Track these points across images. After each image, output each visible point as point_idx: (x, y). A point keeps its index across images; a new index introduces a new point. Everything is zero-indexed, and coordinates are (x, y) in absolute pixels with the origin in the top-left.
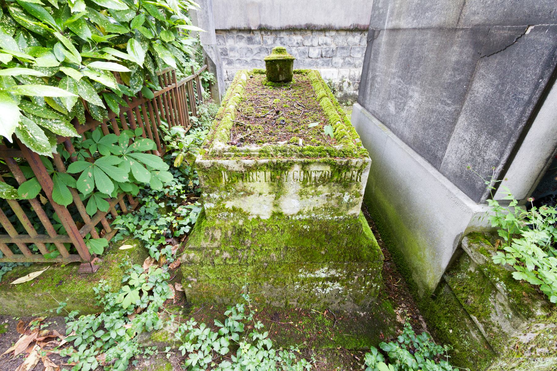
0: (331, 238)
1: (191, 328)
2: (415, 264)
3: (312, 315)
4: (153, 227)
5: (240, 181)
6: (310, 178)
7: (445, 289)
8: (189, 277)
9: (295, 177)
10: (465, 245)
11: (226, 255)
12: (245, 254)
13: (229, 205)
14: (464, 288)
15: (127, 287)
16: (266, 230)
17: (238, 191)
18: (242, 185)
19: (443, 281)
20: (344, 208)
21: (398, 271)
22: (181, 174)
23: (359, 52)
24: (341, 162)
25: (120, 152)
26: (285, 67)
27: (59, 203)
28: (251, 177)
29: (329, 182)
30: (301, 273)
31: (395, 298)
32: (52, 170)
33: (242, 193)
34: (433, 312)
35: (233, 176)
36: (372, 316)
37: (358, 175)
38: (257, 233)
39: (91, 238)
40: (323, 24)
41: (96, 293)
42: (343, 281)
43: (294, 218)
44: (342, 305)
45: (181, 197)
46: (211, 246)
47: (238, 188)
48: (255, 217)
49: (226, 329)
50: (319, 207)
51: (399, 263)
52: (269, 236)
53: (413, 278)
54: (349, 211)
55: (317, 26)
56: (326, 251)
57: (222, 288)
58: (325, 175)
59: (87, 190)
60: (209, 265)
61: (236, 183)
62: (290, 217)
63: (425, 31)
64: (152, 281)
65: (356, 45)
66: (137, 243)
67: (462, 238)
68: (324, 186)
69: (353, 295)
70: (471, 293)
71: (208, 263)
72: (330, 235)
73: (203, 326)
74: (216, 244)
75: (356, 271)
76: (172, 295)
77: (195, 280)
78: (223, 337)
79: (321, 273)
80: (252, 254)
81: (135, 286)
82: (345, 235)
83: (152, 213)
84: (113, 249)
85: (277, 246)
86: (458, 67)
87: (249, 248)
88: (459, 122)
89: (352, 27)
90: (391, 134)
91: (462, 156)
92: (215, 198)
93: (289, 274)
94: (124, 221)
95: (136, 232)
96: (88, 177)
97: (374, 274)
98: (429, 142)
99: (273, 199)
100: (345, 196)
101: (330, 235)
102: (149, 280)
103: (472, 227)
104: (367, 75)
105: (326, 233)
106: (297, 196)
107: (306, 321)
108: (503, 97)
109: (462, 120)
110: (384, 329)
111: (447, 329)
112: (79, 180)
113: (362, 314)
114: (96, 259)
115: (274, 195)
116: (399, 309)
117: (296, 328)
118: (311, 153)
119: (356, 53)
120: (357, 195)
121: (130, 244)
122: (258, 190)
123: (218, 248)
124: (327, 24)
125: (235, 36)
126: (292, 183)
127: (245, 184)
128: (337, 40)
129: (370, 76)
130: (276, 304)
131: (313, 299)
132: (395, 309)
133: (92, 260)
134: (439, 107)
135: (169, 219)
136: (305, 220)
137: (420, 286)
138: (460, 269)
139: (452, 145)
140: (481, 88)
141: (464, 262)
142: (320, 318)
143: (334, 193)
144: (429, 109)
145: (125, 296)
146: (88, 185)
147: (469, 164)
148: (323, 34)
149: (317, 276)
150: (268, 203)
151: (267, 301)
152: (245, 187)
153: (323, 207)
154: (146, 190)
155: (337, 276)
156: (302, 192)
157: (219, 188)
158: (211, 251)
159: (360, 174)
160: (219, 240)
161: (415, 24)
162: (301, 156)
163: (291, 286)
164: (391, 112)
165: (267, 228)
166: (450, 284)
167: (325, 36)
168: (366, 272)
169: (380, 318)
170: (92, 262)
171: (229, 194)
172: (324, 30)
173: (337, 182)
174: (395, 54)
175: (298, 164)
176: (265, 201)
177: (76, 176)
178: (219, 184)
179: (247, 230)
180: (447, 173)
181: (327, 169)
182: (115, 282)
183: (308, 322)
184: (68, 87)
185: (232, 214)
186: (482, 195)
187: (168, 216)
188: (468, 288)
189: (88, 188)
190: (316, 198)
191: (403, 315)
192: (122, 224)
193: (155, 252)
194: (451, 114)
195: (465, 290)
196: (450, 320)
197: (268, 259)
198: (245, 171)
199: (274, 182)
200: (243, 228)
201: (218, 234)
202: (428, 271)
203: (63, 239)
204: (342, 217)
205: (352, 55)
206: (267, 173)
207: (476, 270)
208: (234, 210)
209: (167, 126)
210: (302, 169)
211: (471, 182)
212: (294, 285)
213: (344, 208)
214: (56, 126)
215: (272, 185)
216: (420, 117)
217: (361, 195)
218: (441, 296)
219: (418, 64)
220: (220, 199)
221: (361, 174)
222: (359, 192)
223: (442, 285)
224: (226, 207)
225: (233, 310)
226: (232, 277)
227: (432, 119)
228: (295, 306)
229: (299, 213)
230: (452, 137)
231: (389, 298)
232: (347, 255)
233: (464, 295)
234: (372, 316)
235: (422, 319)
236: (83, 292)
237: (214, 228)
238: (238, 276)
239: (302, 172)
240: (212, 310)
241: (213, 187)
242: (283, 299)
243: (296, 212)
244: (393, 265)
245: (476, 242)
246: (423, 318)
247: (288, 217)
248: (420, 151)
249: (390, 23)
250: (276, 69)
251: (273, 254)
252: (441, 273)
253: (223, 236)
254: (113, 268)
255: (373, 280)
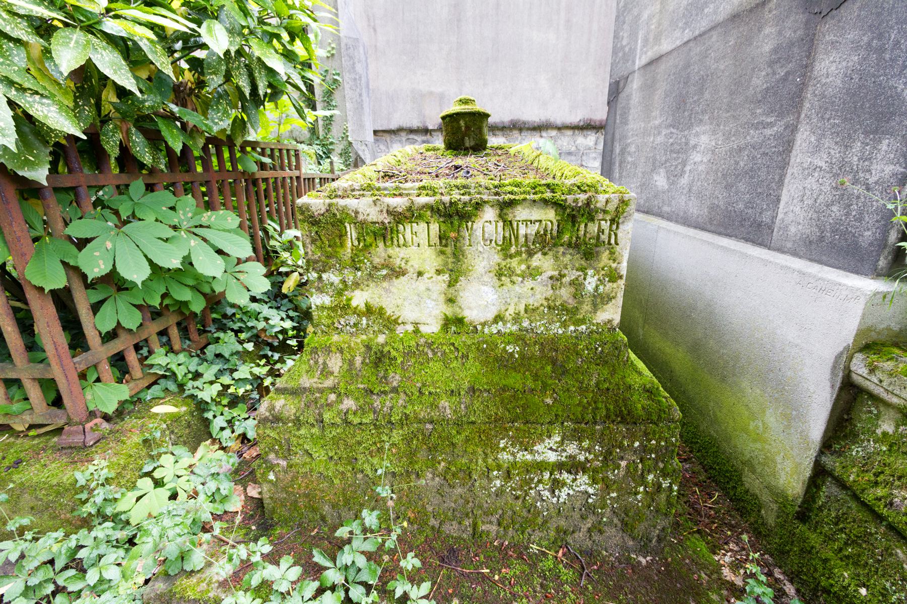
0: (563, 373)
1: (256, 558)
2: (746, 453)
3: (530, 557)
4: (226, 380)
5: (381, 244)
6: (517, 238)
7: (828, 489)
8: (272, 456)
9: (486, 236)
10: (859, 367)
11: (349, 403)
12: (388, 403)
13: (359, 299)
14: (876, 475)
15: (148, 480)
16: (430, 355)
17: (375, 268)
18: (383, 254)
19: (820, 472)
20: (586, 307)
21: (709, 478)
22: (292, 306)
23: (595, 159)
24: (576, 201)
25: (175, 221)
26: (475, 124)
27: (35, 282)
28: (400, 236)
29: (555, 245)
30: (504, 449)
31: (711, 530)
32: (40, 231)
33: (384, 272)
34: (807, 551)
35: (368, 234)
36: (667, 565)
37: (611, 230)
38: (413, 360)
39: (98, 380)
40: (537, 120)
41: (78, 485)
42: (595, 471)
43: (486, 330)
44: (596, 537)
45: (288, 342)
46: (320, 386)
47: (377, 261)
48: (410, 328)
49: (338, 574)
50: (536, 304)
51: (709, 460)
52: (436, 366)
53: (747, 485)
54: (598, 313)
55: (528, 122)
56: (555, 399)
57: (336, 481)
58: (545, 230)
59: (96, 270)
60: (313, 425)
61: (372, 250)
62: (479, 328)
63: (707, 36)
64: (201, 474)
65: (590, 149)
66: (189, 405)
67: (850, 358)
68: (545, 254)
69: (620, 508)
70: (897, 483)
71: (311, 420)
72: (562, 366)
73: (286, 561)
74: (329, 383)
75: (621, 447)
76: (236, 504)
77: (284, 463)
78: (328, 592)
79: (547, 451)
80: (401, 402)
81: (165, 480)
82: (593, 366)
83: (227, 355)
84: (139, 411)
85: (453, 386)
86: (779, 55)
87: (395, 390)
88: (798, 142)
89: (581, 124)
90: (664, 223)
91: (815, 201)
92: (332, 284)
93: (480, 450)
94: (169, 361)
95: (190, 384)
96: (103, 250)
97: (664, 454)
98: (741, 206)
99: (445, 286)
100: (589, 279)
101: (562, 366)
102: (196, 470)
103: (869, 329)
104: (612, 151)
105: (554, 362)
106: (490, 278)
107: (517, 569)
108: (887, 56)
109: (804, 137)
110: (698, 594)
111: (852, 588)
112: (84, 250)
113: (644, 561)
114: (98, 420)
115: (446, 277)
116: (724, 555)
117: (494, 582)
118: (515, 189)
119: (591, 161)
120: (614, 276)
121: (176, 406)
122: (415, 264)
123: (333, 389)
124: (543, 119)
125: (404, 139)
126: (480, 249)
127: (390, 251)
128: (559, 142)
129: (617, 150)
130: (451, 529)
131: (530, 519)
132: (715, 553)
133: (87, 421)
134: (754, 136)
135: (257, 371)
136: (511, 334)
137: (765, 497)
138: (856, 436)
139: (790, 192)
140: (832, 67)
141: (864, 417)
142: (550, 564)
143: (566, 272)
144: (731, 150)
145: (138, 499)
146: (101, 262)
147: (835, 208)
148: (538, 134)
149: (539, 458)
150: (435, 295)
151: (433, 522)
152: (390, 257)
153: (546, 304)
154: (225, 321)
155: (582, 458)
156: (501, 269)
157: (340, 261)
158: (318, 395)
159: (614, 227)
160: (336, 374)
161: (688, 35)
162: (497, 194)
163: (485, 482)
164: (660, 189)
165: (433, 350)
166: (838, 471)
167: (541, 137)
168: (644, 449)
169: (684, 570)
170: (88, 426)
171: (359, 273)
172: (539, 128)
173: (569, 245)
174: (656, 98)
175: (492, 206)
176: (428, 289)
177: (82, 244)
178: (341, 251)
179: (394, 353)
180: (789, 245)
181: (550, 215)
182: (124, 468)
183: (523, 572)
184: (73, 42)
185: (364, 321)
186: (879, 255)
187: (258, 365)
188: (887, 472)
189: (99, 266)
190: (529, 283)
191: (736, 566)
192: (164, 365)
193: (222, 429)
194: (778, 137)
195: (881, 478)
196: (856, 564)
197: (435, 414)
198: (389, 223)
199: (446, 246)
200: (386, 349)
201: (335, 363)
202: (779, 459)
203: (38, 371)
204: (584, 327)
205: (584, 163)
206: (432, 226)
207: (897, 426)
208: (369, 310)
209: (278, 228)
210: (500, 216)
211: (846, 240)
212: (490, 480)
213: (586, 307)
214: (40, 109)
215: (442, 253)
216: (716, 172)
217: (621, 277)
218: (820, 509)
219: (701, 91)
220: (341, 286)
221: (617, 227)
222: (616, 270)
223: (819, 482)
224: (354, 303)
225: (355, 526)
226: (360, 457)
227: (742, 164)
228: (493, 534)
229: (498, 318)
230: (788, 175)
231: (699, 532)
232: (600, 405)
233: (880, 492)
234: (667, 565)
235: (781, 577)
236: (54, 482)
237: (328, 350)
238: (371, 453)
239: (501, 224)
240: (314, 537)
241: (328, 257)
242: (467, 515)
243: (490, 316)
244: (698, 468)
245: (885, 358)
246: (784, 573)
247: (475, 327)
248: (726, 228)
249: (644, 57)
250: (460, 128)
251: (444, 403)
252: (813, 453)
253: (346, 367)
254: (129, 442)
255: (662, 470)
